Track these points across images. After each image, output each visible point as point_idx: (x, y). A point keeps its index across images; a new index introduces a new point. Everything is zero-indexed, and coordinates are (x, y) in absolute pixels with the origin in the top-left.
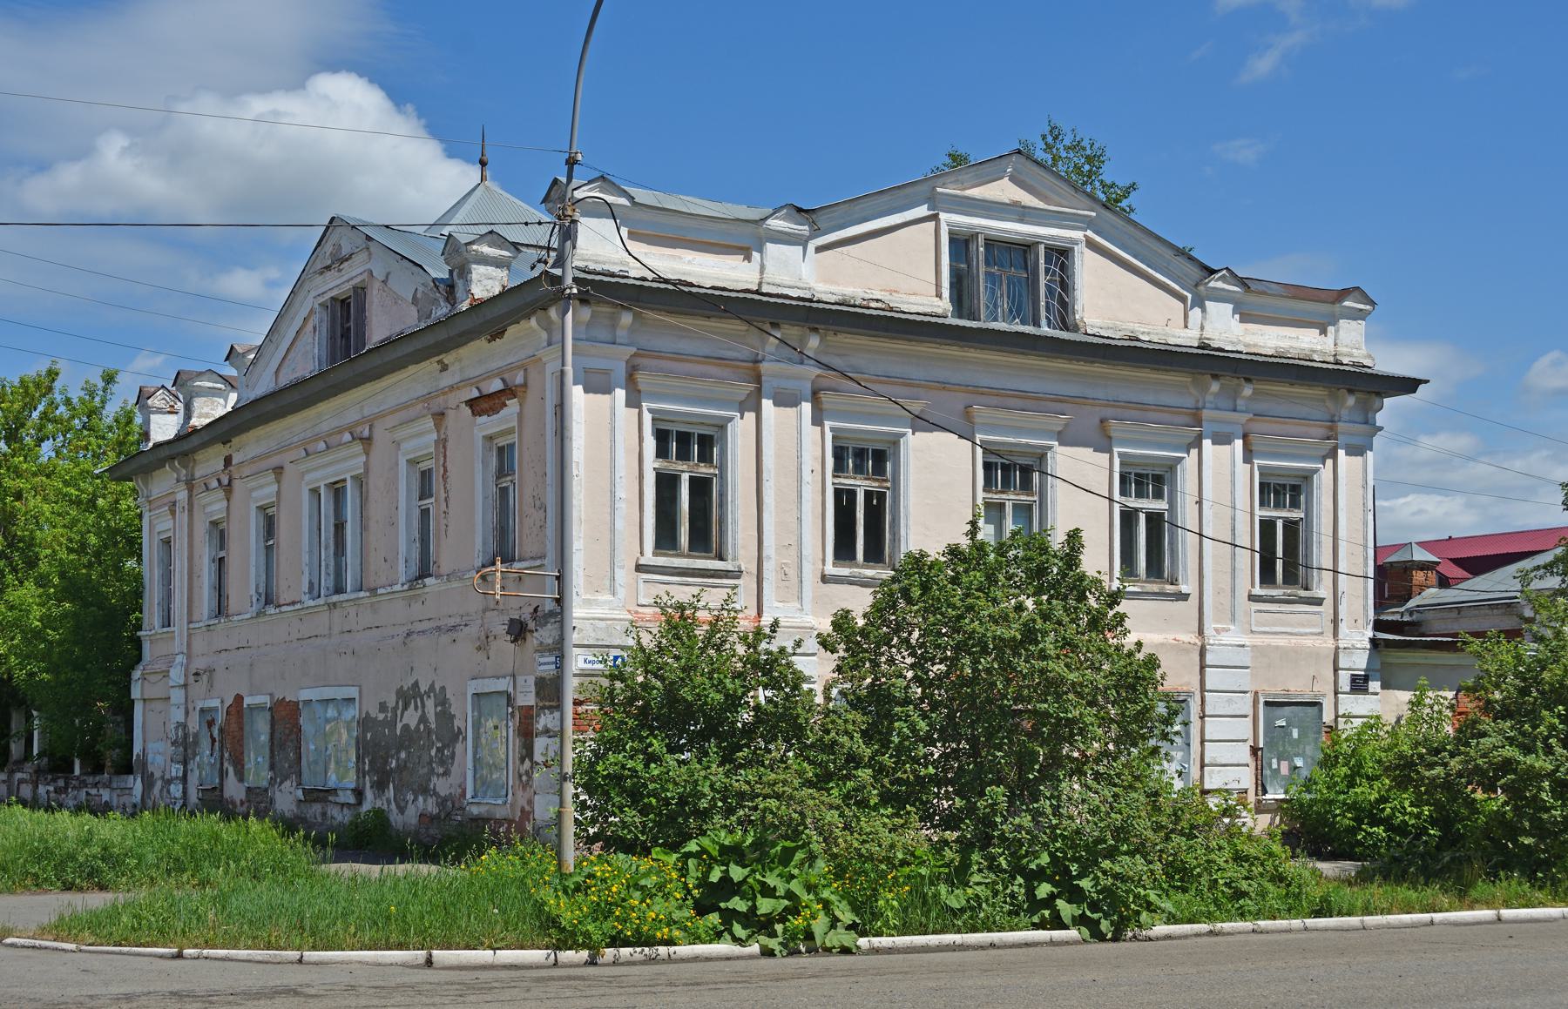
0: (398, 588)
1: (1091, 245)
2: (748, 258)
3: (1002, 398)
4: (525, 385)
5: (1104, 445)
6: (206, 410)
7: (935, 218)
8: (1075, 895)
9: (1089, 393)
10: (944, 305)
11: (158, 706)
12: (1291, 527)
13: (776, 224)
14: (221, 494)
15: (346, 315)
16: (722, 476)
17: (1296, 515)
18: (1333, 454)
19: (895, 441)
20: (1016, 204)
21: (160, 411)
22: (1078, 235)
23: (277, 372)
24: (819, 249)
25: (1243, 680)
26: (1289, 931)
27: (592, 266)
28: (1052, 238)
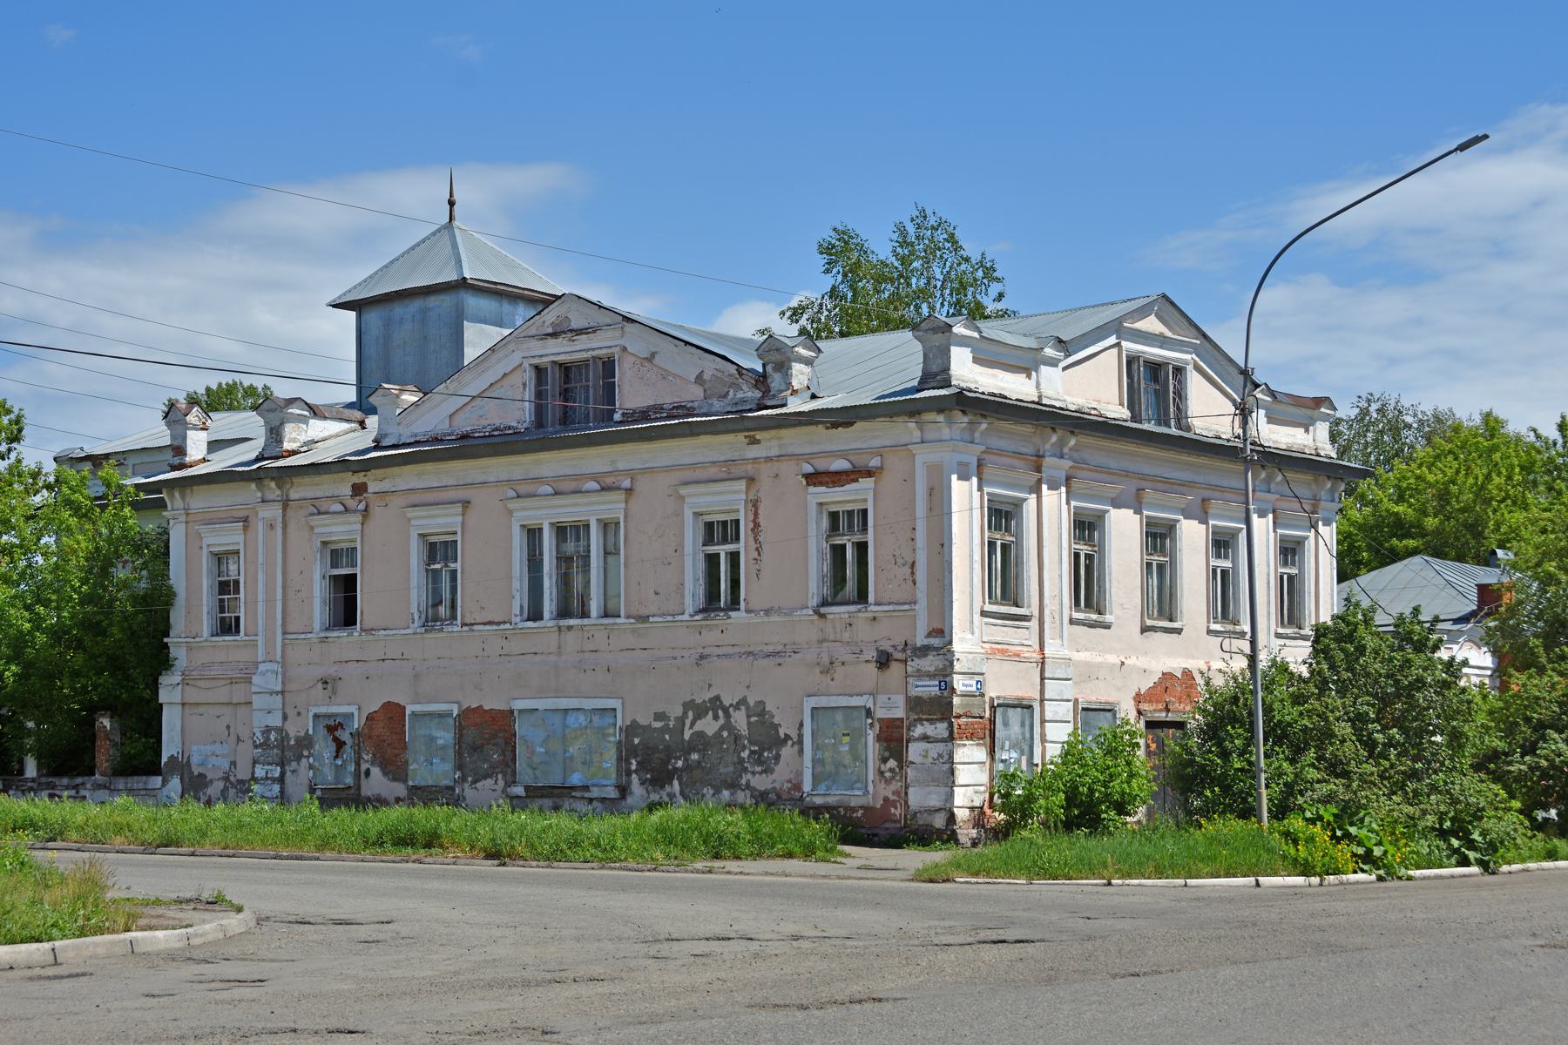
0: (686, 617)
1: (1197, 368)
2: (1029, 377)
3: (1167, 485)
4: (881, 468)
5: (1204, 521)
6: (294, 435)
7: (1118, 345)
8: (1471, 845)
9: (1197, 478)
10: (1124, 413)
11: (242, 711)
13: (1049, 352)
14: (359, 518)
16: (1173, 562)
17: (1294, 571)
18: (1314, 526)
19: (1101, 516)
20: (1161, 335)
21: (195, 428)
22: (1188, 357)
24: (1064, 369)
25: (1068, 690)
28: (1177, 360)
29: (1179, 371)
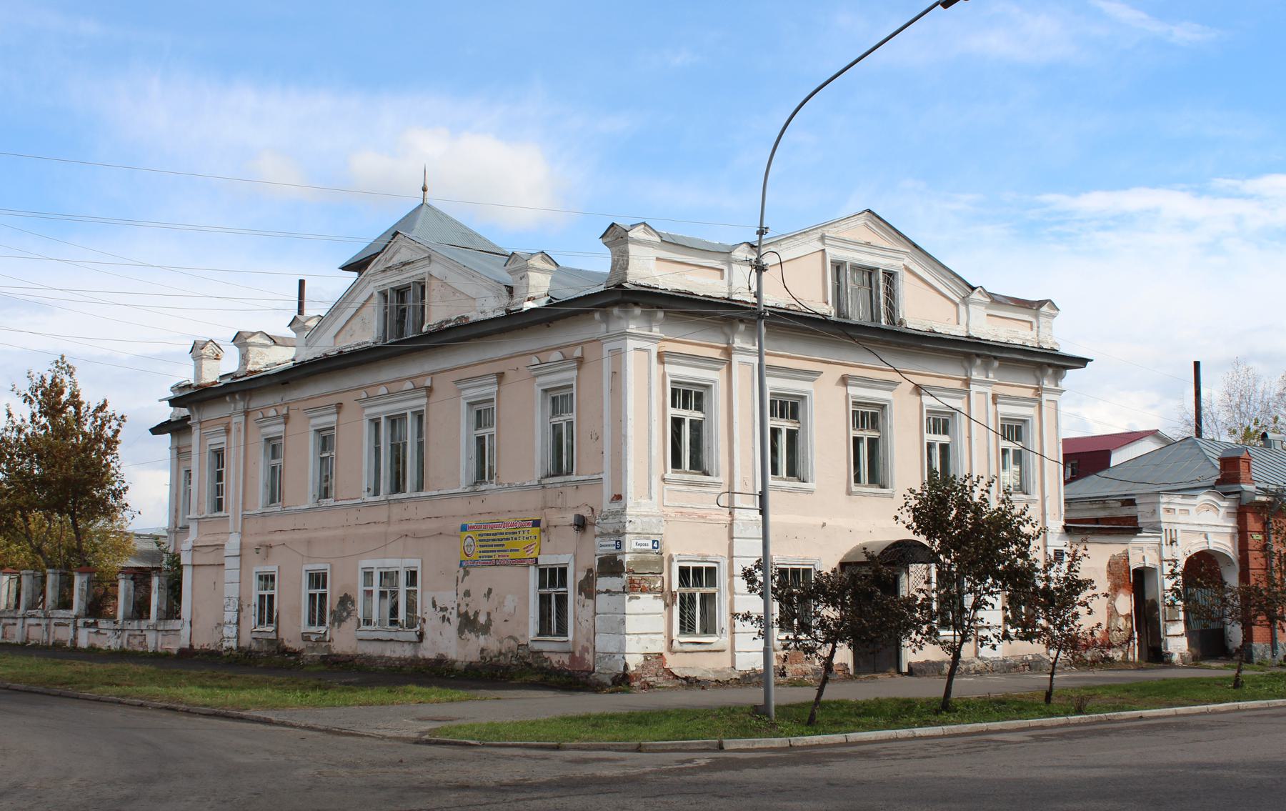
12: (944, 448)
15: (403, 301)
16: (885, 436)
21: (209, 358)
23: (335, 337)
26: (896, 739)
27: (638, 282)
29: (890, 276)
